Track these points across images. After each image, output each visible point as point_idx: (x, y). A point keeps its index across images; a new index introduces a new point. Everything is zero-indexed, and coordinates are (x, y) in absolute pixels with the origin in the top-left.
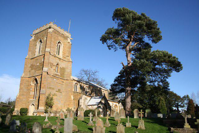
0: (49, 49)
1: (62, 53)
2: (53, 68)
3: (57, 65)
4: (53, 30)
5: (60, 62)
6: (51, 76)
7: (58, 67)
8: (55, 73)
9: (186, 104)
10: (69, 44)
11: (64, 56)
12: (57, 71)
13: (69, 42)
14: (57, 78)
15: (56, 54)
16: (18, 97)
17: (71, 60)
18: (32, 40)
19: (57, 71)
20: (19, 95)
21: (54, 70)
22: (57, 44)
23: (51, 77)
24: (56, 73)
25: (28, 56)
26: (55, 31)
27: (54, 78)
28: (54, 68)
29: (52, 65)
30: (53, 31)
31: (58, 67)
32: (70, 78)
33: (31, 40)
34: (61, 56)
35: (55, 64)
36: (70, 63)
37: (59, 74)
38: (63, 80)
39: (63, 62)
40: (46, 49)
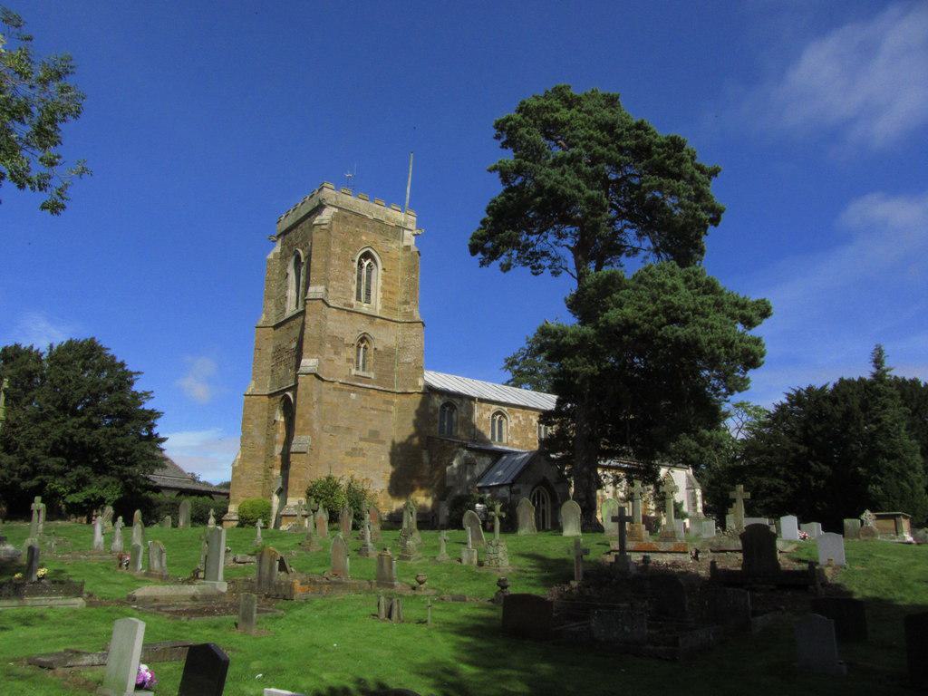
0: (321, 289)
1: (380, 295)
2: (344, 355)
3: (362, 340)
4: (336, 210)
5: (371, 332)
6: (339, 386)
7: (365, 348)
8: (354, 372)
9: (147, 671)
10: (408, 254)
11: (390, 304)
12: (361, 363)
13: (407, 248)
14: (356, 389)
15: (353, 301)
16: (236, 465)
17: (417, 317)
18: (275, 254)
19: (361, 363)
20: (239, 457)
21: (349, 360)
22: (356, 265)
23: (334, 389)
24: (361, 373)
25: (264, 317)
26: (345, 215)
27: (350, 391)
28: (351, 353)
29: (337, 343)
30: (335, 218)
31: (365, 348)
32: (416, 386)
33: (271, 256)
34: (376, 305)
35: (352, 338)
36: (418, 329)
37: (372, 375)
38: (388, 397)
39: (384, 325)
40: (311, 289)
